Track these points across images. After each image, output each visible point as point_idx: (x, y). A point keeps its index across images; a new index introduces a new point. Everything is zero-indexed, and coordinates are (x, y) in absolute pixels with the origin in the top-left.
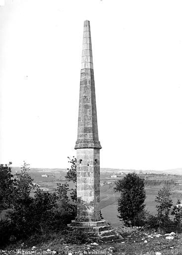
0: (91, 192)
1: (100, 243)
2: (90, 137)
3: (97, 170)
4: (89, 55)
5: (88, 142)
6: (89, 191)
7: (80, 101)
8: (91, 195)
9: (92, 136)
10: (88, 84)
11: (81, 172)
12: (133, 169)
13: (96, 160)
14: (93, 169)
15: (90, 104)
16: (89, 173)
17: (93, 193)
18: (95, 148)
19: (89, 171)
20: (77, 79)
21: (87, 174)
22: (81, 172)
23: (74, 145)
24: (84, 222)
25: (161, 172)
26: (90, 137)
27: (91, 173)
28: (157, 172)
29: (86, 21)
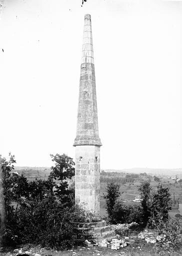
0: (91, 191)
1: (121, 248)
2: (88, 135)
3: (97, 167)
4: (90, 49)
5: (89, 139)
6: (89, 190)
7: (80, 97)
8: (91, 194)
9: (92, 133)
10: (89, 79)
11: (80, 169)
12: (44, 167)
13: (96, 158)
14: (94, 166)
15: (91, 100)
16: (89, 171)
17: (94, 192)
18: (96, 145)
19: (89, 169)
20: (77, 73)
21: (87, 171)
22: (80, 169)
23: (73, 143)
24: (105, 227)
25: (114, 170)
26: (88, 135)
27: (91, 171)
28: (118, 171)
29: (87, 15)
